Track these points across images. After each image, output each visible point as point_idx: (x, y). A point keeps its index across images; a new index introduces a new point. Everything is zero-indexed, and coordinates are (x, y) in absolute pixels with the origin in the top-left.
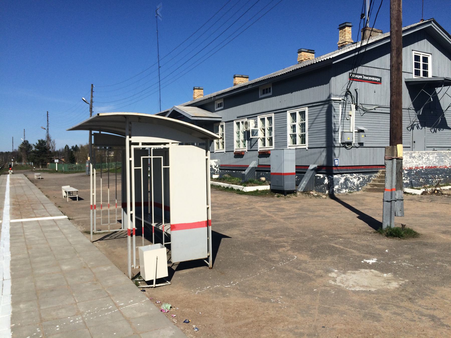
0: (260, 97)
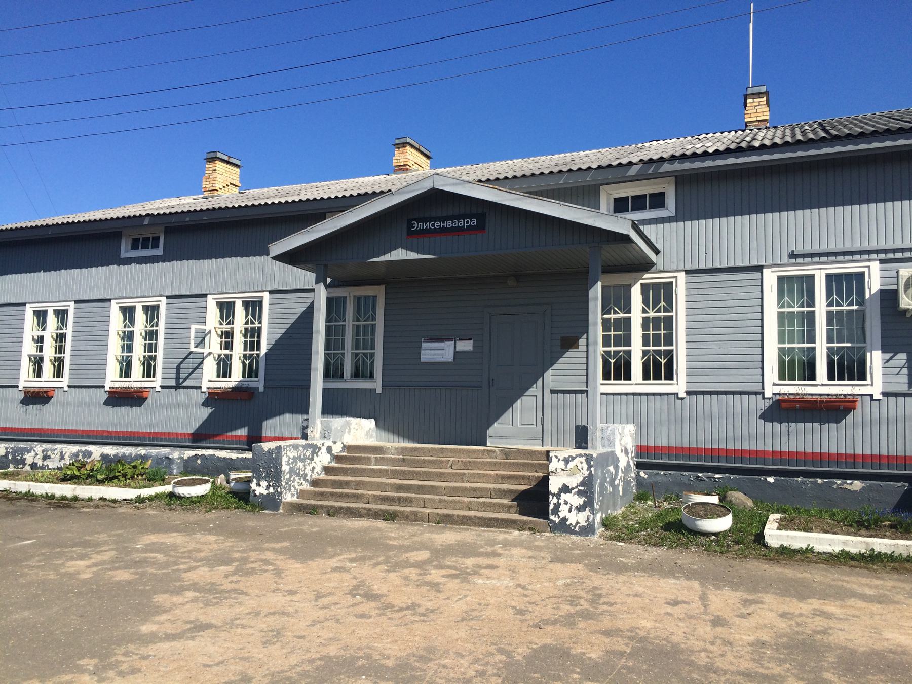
0: (124, 255)
